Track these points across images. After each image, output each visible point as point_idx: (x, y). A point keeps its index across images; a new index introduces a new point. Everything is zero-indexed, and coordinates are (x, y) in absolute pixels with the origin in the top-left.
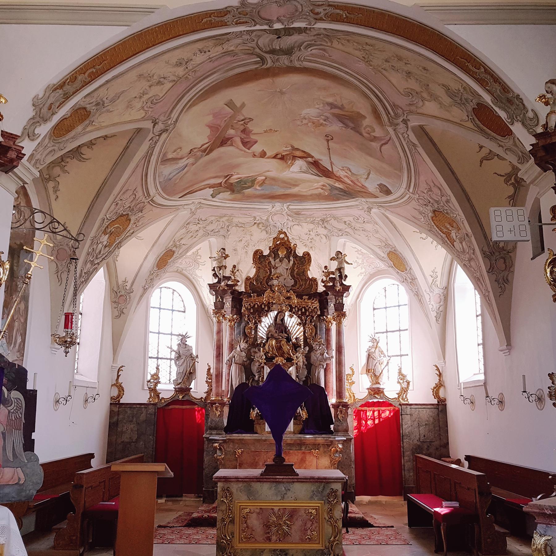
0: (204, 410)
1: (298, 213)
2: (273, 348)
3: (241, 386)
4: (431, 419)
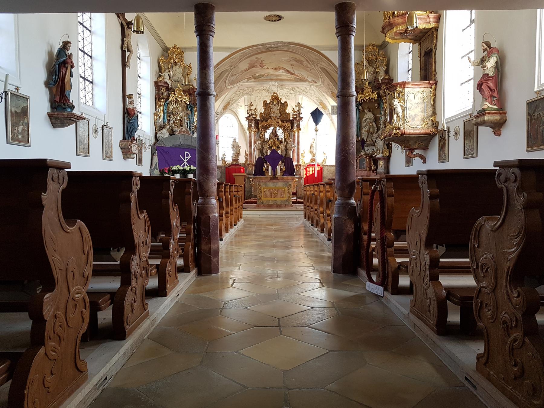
1: (282, 85)
2: (272, 143)
3: (259, 158)
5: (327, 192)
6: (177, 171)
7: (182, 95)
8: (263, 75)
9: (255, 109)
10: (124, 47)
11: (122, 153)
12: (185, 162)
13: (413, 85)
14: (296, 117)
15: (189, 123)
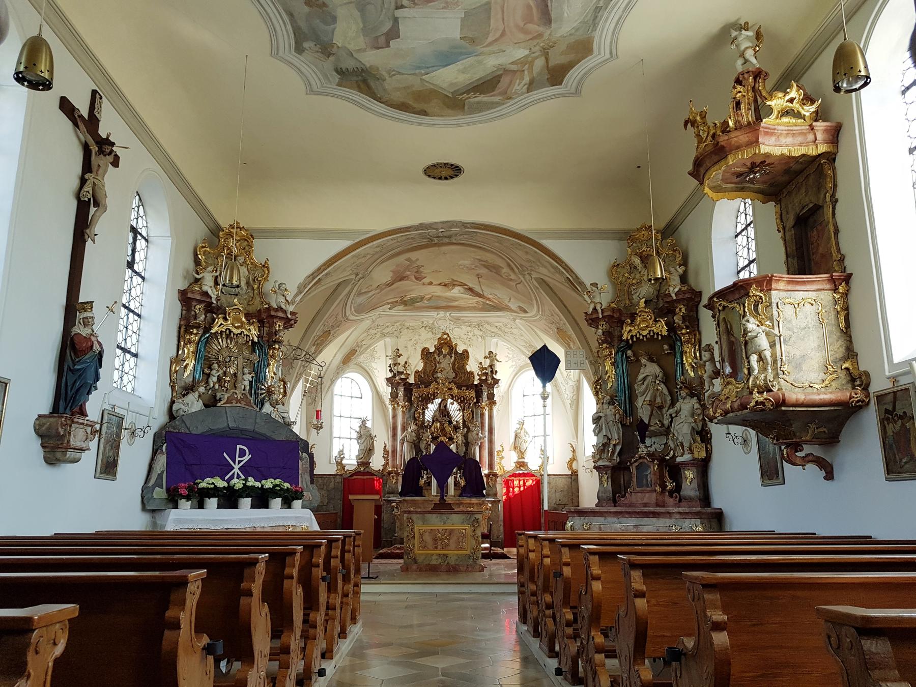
0: (381, 480)
1: (458, 319)
3: (412, 460)
4: (566, 487)
5: (636, 596)
7: (242, 323)
8: (422, 299)
9: (406, 363)
10: (82, 191)
11: (43, 447)
12: (236, 470)
14: (486, 379)
15: (256, 381)
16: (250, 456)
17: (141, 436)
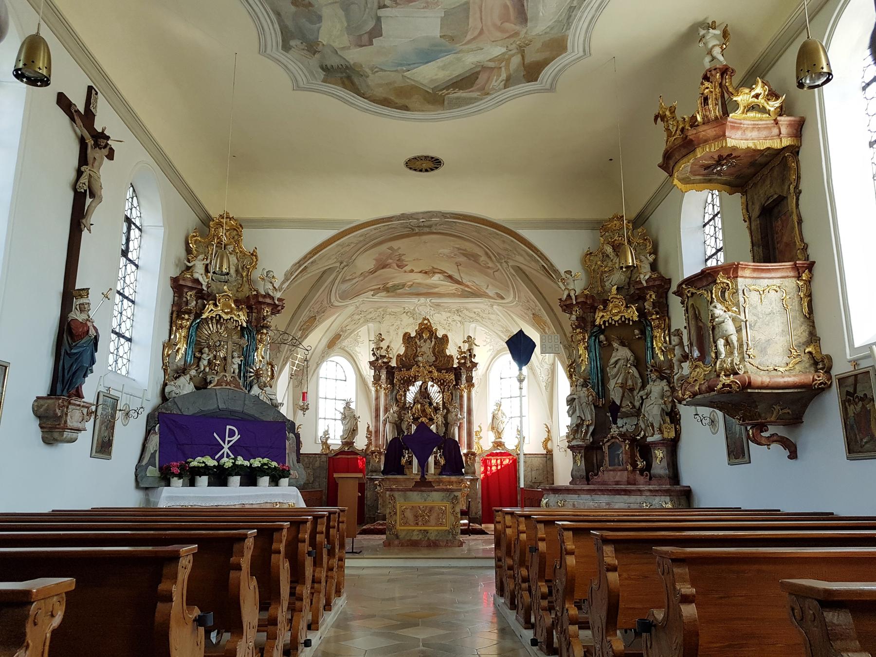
0: (364, 459)
1: (438, 305)
3: (394, 440)
4: (541, 465)
5: (608, 570)
6: (202, 471)
7: (232, 309)
8: (404, 285)
9: (388, 347)
10: (79, 183)
11: (41, 427)
12: (226, 449)
13: (755, 270)
14: (465, 362)
15: (245, 365)
16: (239, 436)
17: (135, 417)
